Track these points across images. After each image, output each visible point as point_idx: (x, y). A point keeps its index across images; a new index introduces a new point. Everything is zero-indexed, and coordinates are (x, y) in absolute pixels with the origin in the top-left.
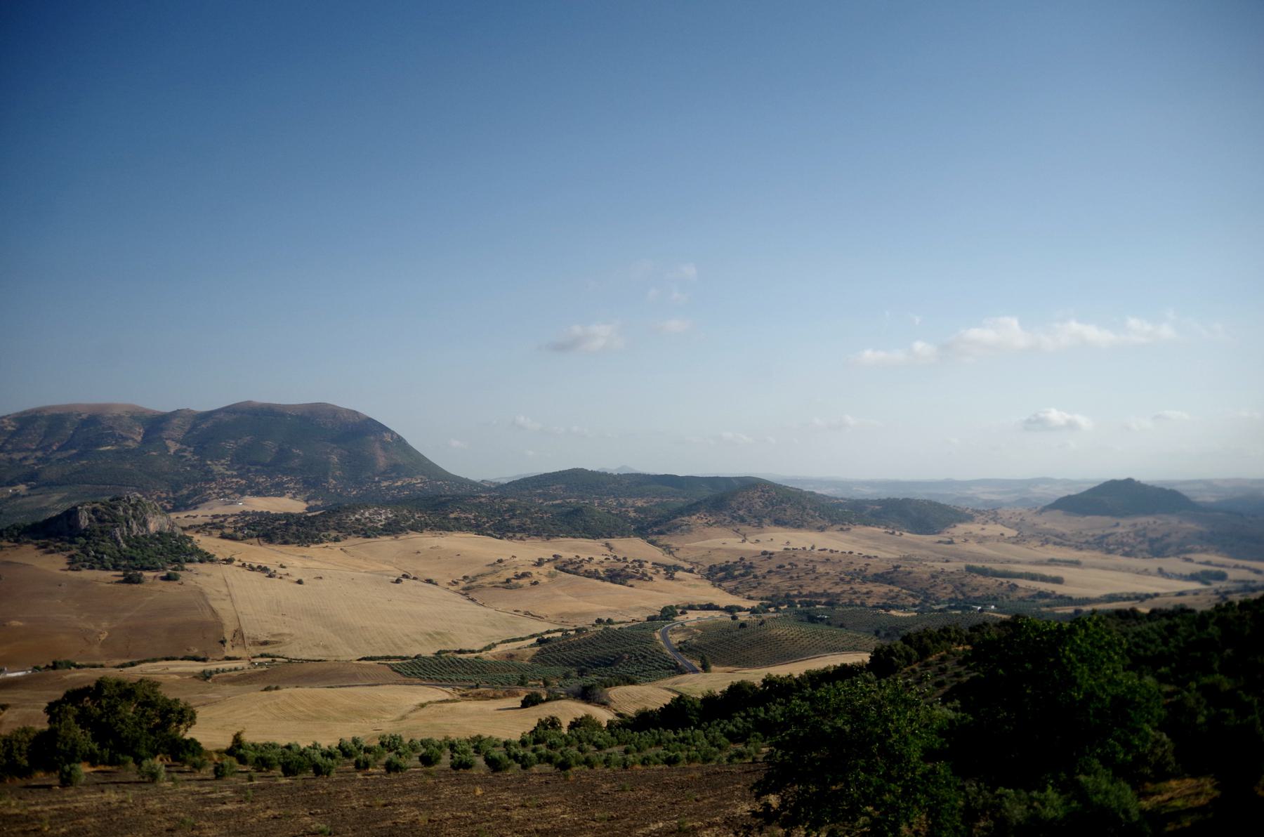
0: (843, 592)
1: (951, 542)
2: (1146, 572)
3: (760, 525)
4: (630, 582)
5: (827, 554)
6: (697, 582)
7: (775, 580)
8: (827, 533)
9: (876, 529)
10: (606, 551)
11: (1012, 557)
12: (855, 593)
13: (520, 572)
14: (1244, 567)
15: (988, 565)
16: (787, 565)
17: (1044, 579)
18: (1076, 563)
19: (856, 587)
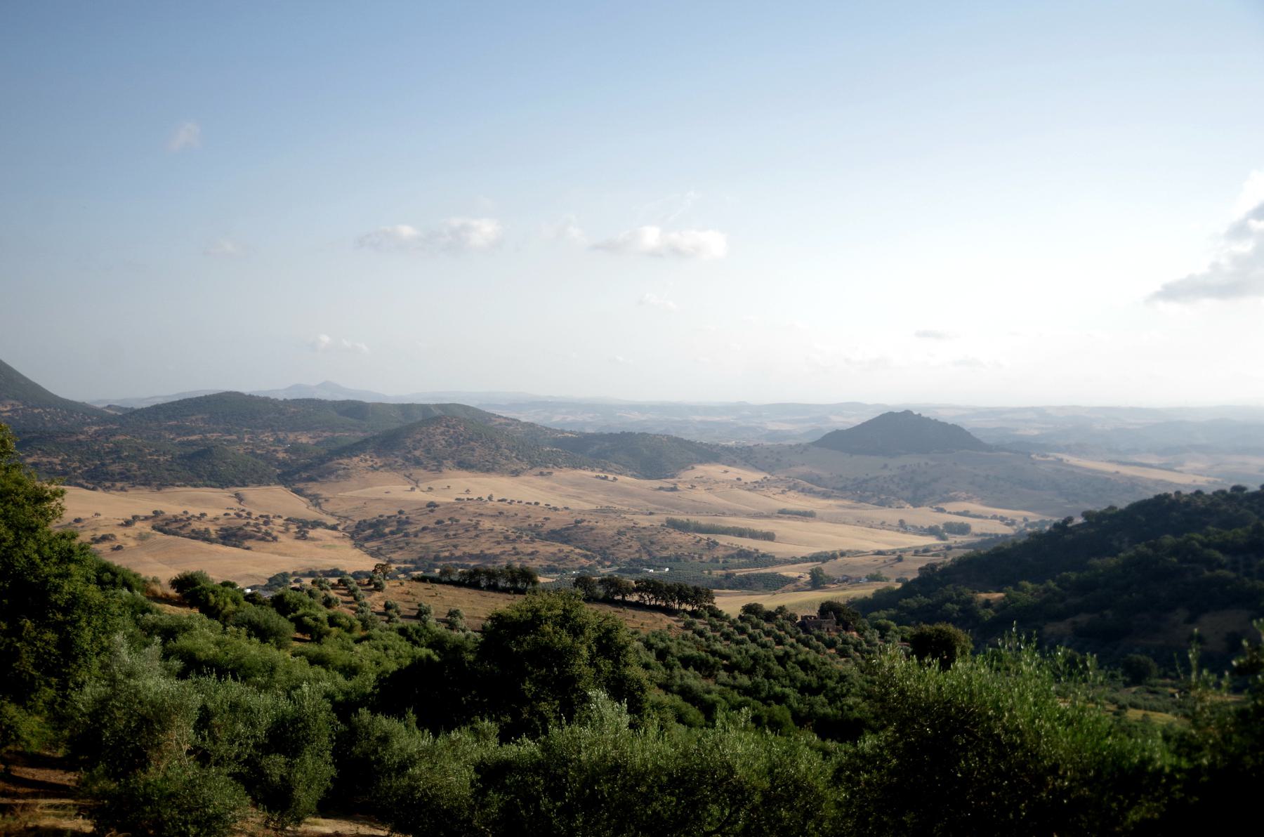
0: (502, 553)
1: (674, 489)
2: (883, 525)
3: (438, 469)
4: (247, 543)
5: (501, 506)
6: (336, 542)
7: (428, 539)
8: (522, 478)
9: (588, 473)
10: (233, 503)
11: (743, 507)
12: (517, 554)
13: (99, 534)
14: (994, 517)
15: (694, 518)
16: (445, 521)
17: (754, 535)
18: (806, 515)
19: (520, 546)
